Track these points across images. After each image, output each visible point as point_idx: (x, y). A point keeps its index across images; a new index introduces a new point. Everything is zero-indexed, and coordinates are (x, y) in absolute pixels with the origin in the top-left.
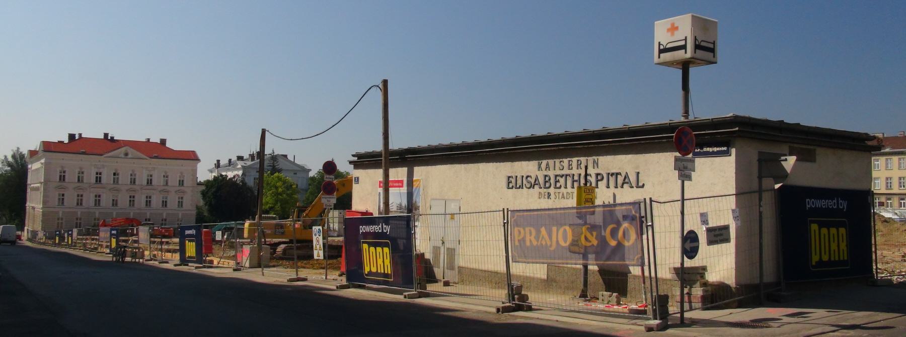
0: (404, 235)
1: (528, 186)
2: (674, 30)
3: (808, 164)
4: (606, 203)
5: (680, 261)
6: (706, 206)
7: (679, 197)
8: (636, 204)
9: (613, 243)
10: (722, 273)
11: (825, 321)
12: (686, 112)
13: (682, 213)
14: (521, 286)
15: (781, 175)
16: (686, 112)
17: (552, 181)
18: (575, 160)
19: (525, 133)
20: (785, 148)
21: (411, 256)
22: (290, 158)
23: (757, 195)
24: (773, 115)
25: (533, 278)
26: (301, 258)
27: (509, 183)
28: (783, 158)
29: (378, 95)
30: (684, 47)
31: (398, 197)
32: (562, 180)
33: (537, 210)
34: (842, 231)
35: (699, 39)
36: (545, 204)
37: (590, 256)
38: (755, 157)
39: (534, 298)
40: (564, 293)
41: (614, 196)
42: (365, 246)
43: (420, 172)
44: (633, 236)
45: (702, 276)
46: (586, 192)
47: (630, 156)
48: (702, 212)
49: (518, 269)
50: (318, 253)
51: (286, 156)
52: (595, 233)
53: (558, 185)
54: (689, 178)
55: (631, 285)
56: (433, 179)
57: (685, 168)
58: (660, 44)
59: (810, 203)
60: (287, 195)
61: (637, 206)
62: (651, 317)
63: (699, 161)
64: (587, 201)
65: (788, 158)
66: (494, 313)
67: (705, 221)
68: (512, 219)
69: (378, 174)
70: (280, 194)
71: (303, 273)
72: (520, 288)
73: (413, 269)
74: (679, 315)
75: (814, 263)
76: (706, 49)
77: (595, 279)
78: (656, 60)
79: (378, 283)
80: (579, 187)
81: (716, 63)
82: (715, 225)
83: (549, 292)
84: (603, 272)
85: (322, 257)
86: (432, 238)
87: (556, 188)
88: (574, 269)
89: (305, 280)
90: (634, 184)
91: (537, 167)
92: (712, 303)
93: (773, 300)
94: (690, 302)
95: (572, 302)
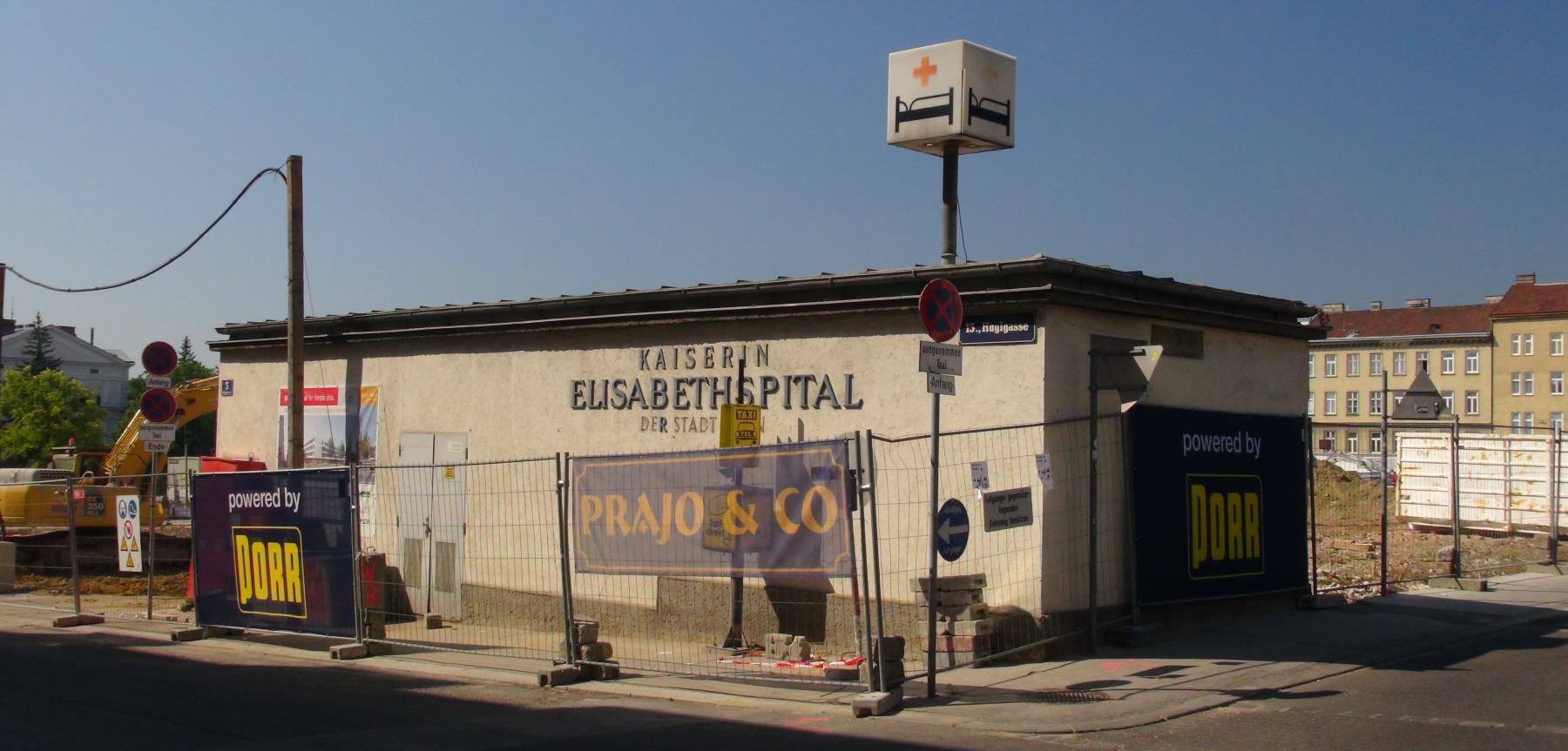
0: (339, 515)
1: (619, 403)
2: (926, 72)
3: (1189, 363)
4: (784, 441)
5: (928, 565)
6: (988, 448)
7: (929, 430)
8: (840, 444)
9: (791, 528)
10: (1014, 588)
11: (1210, 683)
12: (951, 248)
13: (935, 463)
14: (596, 626)
15: (1134, 384)
16: (951, 248)
17: (671, 393)
18: (719, 347)
19: (613, 286)
20: (1144, 330)
21: (350, 561)
22: (82, 334)
23: (1087, 424)
24: (1121, 260)
25: (630, 607)
26: (89, 570)
27: (577, 396)
28: (1138, 349)
29: (282, 190)
30: (946, 110)
31: (323, 429)
32: (691, 391)
33: (632, 457)
34: (1252, 498)
35: (979, 94)
36: (654, 442)
37: (746, 556)
38: (1085, 347)
39: (624, 650)
40: (690, 640)
41: (801, 425)
42: (242, 540)
43: (375, 369)
44: (832, 509)
45: (977, 595)
46: (740, 419)
47: (833, 341)
48: (975, 460)
49: (587, 587)
50: (130, 558)
51: (70, 330)
52: (752, 507)
53: (683, 402)
54: (949, 388)
55: (833, 616)
56: (405, 385)
57: (942, 366)
58: (898, 101)
59: (1192, 443)
60: (73, 421)
61: (841, 447)
62: (868, 685)
63: (970, 354)
64: (742, 436)
65: (1148, 349)
66: (534, 687)
67: (981, 482)
68: (575, 477)
69: (276, 374)
70: (56, 419)
71: (93, 605)
72: (593, 629)
73: (359, 594)
74: (925, 680)
75: (1196, 566)
76: (991, 117)
77: (759, 606)
78: (891, 135)
79: (274, 624)
80: (727, 407)
81: (1011, 147)
82: (1001, 489)
83: (659, 637)
84: (775, 590)
85: (138, 568)
86: (403, 521)
87: (677, 407)
88: (714, 585)
89: (98, 621)
90: (841, 401)
91: (637, 361)
92: (994, 652)
93: (1117, 643)
94: (951, 651)
95: (703, 657)
